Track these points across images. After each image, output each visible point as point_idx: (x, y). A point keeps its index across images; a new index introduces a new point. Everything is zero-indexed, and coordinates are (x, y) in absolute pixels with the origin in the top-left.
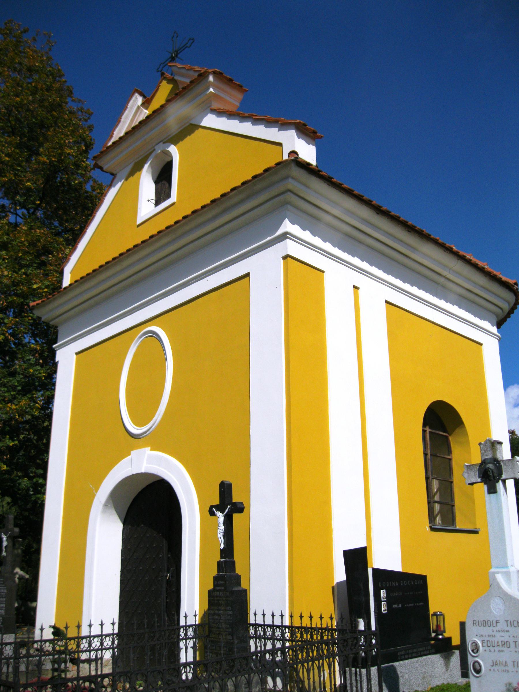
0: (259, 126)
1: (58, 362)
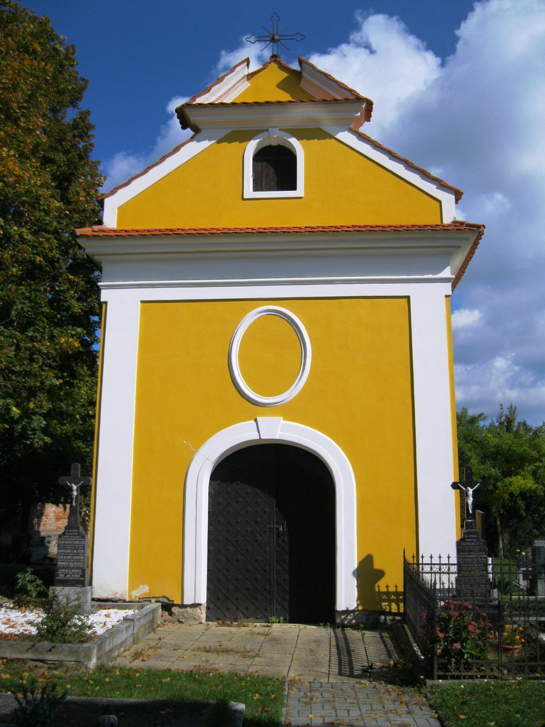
0: (354, 136)
1: (106, 303)
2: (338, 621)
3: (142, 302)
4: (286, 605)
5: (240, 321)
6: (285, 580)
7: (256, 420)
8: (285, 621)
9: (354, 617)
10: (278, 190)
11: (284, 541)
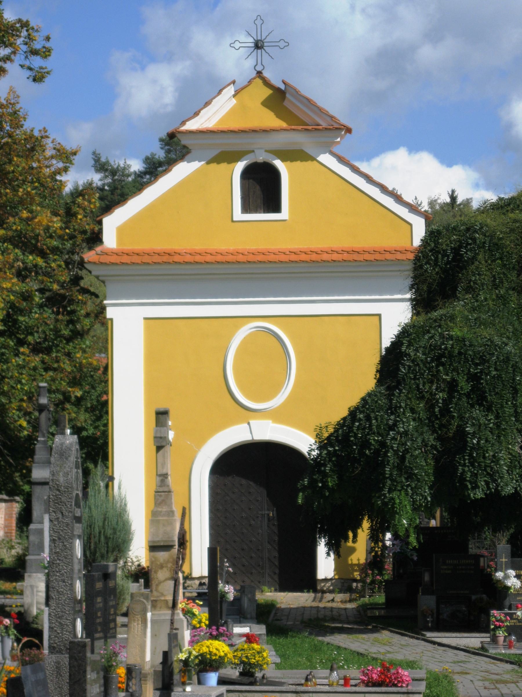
2: (319, 588)
3: (145, 319)
4: (276, 577)
5: (231, 339)
6: (275, 557)
7: (249, 424)
8: (276, 590)
9: (332, 584)
10: (265, 212)
11: (274, 525)
